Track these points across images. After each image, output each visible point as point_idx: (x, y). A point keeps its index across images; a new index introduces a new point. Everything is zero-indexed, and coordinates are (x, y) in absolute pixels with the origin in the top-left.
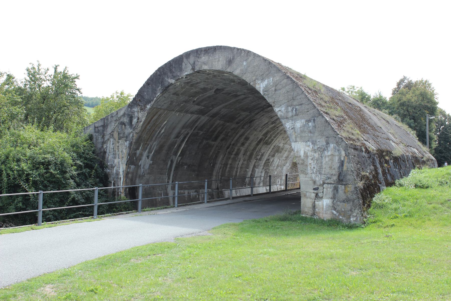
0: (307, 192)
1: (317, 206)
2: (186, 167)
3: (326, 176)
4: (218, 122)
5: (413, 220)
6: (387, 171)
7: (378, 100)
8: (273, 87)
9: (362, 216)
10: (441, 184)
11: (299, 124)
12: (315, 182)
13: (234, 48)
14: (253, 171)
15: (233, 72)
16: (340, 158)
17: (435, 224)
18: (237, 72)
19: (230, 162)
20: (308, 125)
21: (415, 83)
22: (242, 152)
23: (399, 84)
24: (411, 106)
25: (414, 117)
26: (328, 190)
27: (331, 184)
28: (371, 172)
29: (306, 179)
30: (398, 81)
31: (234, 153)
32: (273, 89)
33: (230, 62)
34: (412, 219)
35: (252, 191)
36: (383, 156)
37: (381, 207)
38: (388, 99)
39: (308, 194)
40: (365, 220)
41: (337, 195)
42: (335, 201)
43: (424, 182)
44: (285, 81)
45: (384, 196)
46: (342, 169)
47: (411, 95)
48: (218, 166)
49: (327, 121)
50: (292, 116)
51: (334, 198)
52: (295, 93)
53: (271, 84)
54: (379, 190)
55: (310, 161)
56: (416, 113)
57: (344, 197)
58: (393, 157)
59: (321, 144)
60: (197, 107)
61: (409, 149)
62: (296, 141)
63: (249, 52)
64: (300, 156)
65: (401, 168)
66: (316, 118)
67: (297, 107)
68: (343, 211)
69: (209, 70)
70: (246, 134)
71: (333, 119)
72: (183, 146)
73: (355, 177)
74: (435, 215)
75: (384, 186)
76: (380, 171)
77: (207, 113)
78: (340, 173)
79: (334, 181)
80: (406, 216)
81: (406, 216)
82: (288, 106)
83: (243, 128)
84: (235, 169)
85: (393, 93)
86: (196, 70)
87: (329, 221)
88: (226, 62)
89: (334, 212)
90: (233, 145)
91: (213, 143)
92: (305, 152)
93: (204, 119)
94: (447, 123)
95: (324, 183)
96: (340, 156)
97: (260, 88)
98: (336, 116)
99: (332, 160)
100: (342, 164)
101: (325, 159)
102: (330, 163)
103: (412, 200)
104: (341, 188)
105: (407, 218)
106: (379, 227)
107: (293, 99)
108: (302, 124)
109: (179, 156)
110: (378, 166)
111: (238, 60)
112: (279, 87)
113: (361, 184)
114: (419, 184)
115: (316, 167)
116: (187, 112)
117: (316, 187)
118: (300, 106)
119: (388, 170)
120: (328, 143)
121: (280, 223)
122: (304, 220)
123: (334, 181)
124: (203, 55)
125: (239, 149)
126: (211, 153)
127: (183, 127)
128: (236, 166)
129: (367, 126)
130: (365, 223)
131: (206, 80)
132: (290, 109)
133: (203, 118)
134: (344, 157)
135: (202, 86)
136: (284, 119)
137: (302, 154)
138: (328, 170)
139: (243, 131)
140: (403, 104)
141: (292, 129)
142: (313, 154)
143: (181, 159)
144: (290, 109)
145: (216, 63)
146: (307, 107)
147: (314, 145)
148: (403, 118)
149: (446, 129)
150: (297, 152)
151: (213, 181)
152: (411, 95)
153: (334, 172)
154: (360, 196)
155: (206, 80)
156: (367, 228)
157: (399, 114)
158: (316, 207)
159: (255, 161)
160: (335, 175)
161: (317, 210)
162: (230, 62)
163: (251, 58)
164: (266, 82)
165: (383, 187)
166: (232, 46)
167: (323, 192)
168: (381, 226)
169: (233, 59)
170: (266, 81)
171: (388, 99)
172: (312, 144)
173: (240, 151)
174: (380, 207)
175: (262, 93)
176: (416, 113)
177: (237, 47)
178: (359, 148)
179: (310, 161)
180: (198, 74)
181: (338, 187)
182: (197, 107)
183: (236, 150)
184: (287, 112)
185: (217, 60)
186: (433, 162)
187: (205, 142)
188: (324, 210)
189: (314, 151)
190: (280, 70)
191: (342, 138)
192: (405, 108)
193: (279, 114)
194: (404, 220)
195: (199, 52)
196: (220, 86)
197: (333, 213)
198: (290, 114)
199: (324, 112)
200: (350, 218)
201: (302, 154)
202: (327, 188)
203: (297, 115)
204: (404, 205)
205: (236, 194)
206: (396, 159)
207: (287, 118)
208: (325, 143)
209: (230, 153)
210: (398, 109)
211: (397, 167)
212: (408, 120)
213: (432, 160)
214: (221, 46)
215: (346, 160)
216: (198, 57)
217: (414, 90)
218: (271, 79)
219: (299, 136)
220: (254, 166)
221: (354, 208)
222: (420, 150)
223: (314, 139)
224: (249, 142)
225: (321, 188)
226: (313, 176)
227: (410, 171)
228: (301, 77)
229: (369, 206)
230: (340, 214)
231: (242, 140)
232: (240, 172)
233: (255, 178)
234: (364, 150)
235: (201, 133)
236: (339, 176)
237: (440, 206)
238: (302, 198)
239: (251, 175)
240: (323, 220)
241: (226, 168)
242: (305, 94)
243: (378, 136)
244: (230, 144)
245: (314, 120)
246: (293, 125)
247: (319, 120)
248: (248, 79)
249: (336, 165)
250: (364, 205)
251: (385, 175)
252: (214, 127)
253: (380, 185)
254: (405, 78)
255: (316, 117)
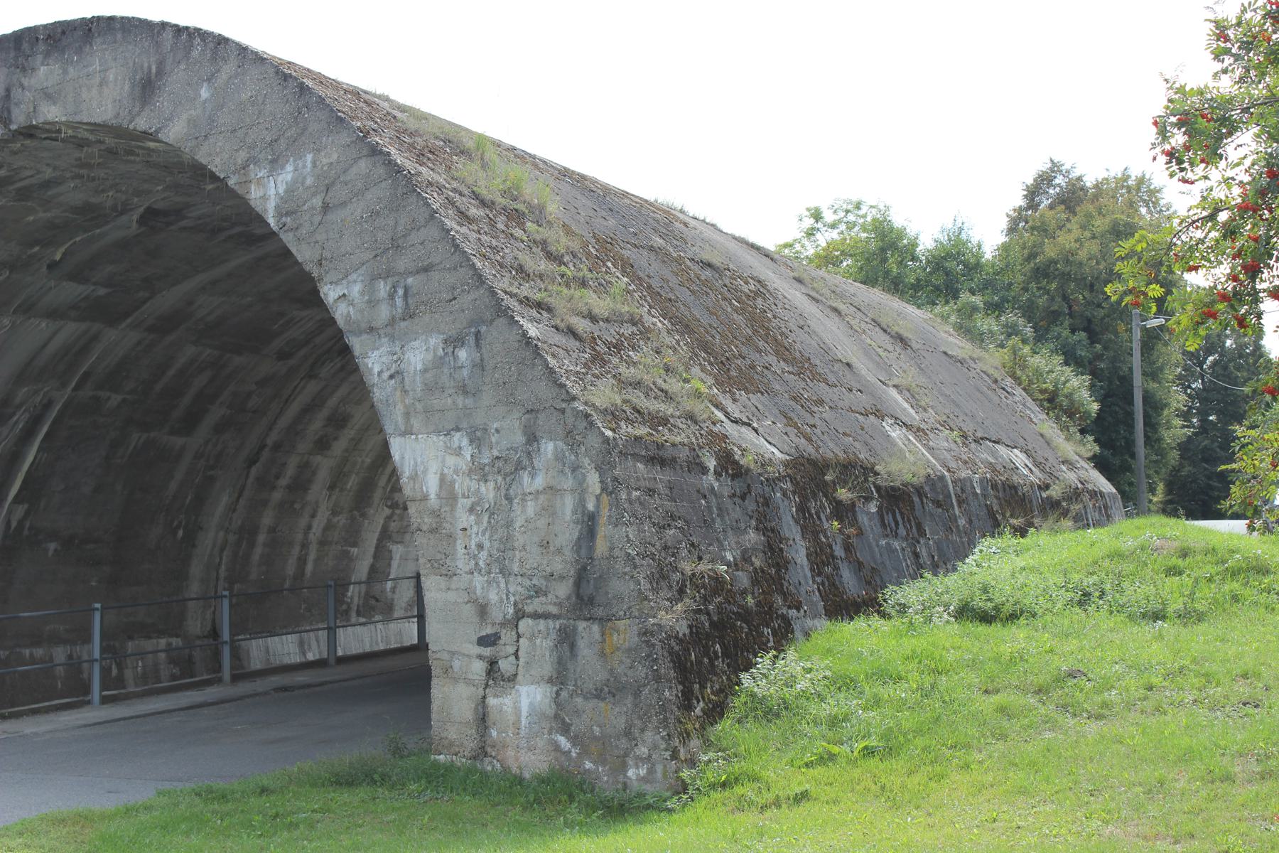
0: (453, 653)
1: (493, 716)
2: (52, 546)
3: (527, 583)
4: (190, 351)
5: (892, 772)
6: (839, 551)
7: (948, 256)
8: (314, 195)
9: (675, 756)
10: (1084, 599)
11: (417, 356)
12: (483, 611)
13: (164, 25)
14: (381, 553)
15: (157, 132)
16: (582, 502)
17: (981, 788)
18: (174, 133)
19: (267, 519)
20: (455, 358)
21: (1096, 186)
22: (323, 476)
23: (1033, 193)
24: (1075, 280)
25: (1089, 321)
26: (537, 643)
27: (546, 616)
28: (746, 558)
29: (451, 596)
30: (1030, 181)
31: (283, 482)
32: (317, 202)
33: (147, 88)
34: (899, 764)
35: (332, 642)
36: (827, 490)
37: (767, 712)
38: (988, 253)
39: (456, 664)
40: (686, 774)
41: (570, 666)
42: (564, 694)
43: (1005, 593)
44: (363, 165)
45: (813, 662)
46: (591, 549)
47: (1076, 232)
48: (209, 540)
49: (526, 340)
50: (392, 322)
51: (559, 679)
52: (402, 222)
53: (309, 181)
54: (784, 636)
55: (464, 519)
56: (1099, 306)
57: (601, 676)
58: (878, 488)
59: (504, 444)
60: (72, 291)
61: (984, 454)
62: (407, 432)
63: (222, 41)
64: (425, 498)
65: (922, 533)
66: (483, 329)
67: (410, 280)
68: (595, 738)
69: (68, 124)
70: (332, 402)
71: (572, 332)
72: (30, 459)
73: (645, 585)
74: (1000, 745)
75: (815, 616)
76: (799, 552)
77: (127, 315)
78: (584, 568)
79: (560, 605)
80: (869, 752)
81: (869, 752)
82: (374, 278)
83: (311, 376)
84: (296, 550)
85: (1012, 230)
86: (14, 127)
87: (543, 781)
88: (133, 86)
89: (563, 741)
90: (277, 447)
91: (179, 441)
92: (442, 479)
93: (118, 340)
94: (1229, 343)
95: (520, 615)
96: (581, 491)
97: (265, 198)
98: (593, 318)
99: (549, 511)
100: (589, 525)
101: (524, 507)
102: (542, 523)
103: (914, 679)
104: (587, 632)
105: (873, 763)
106: (742, 805)
107: (396, 246)
108: (430, 357)
109: (17, 500)
110: (791, 529)
111: (177, 76)
112: (340, 193)
113: (674, 618)
114: (979, 603)
115: (487, 544)
116: (28, 309)
117: (489, 630)
118: (422, 277)
119: (848, 548)
120: (532, 438)
121: (344, 796)
122: (440, 780)
123: (560, 605)
124: (40, 57)
125: (304, 466)
126: (173, 486)
127: (21, 377)
128: (300, 536)
129: (772, 359)
130: (685, 790)
131: (83, 172)
132: (383, 288)
133: (111, 335)
134: (598, 498)
135: (72, 194)
136: (359, 333)
137: (432, 485)
138: (534, 558)
139: (312, 387)
140: (1042, 273)
141: (391, 377)
142: (474, 485)
143: (27, 513)
144: (383, 288)
145: (94, 91)
146: (450, 279)
147: (479, 447)
148: (1042, 326)
149: (1225, 368)
150: (414, 477)
151: (191, 604)
152: (1076, 232)
153: (558, 566)
154: (666, 669)
155: (83, 172)
156: (689, 814)
157: (1028, 312)
158: (490, 723)
159: (387, 511)
160: (562, 578)
161: (494, 733)
162: (147, 88)
163: (228, 69)
164: (287, 174)
165: (809, 622)
166: (154, 14)
167: (516, 655)
168: (751, 803)
169: (160, 73)
170: (289, 168)
171: (988, 253)
172: (471, 441)
173: (314, 473)
174: (766, 714)
175: (272, 221)
176: (1099, 306)
177: (174, 22)
178: (683, 454)
179: (464, 519)
180: (28, 142)
181: (575, 629)
182: (72, 291)
183: (290, 471)
184: (373, 303)
185: (98, 80)
186: (1100, 504)
187: (136, 438)
188: (523, 733)
189: (480, 472)
190: (341, 119)
191: (587, 416)
192: (1054, 286)
193: (341, 313)
194: (856, 773)
195: (25, 46)
196: (159, 196)
197: (557, 748)
198: (384, 312)
199: (526, 302)
200: (624, 767)
201: (432, 485)
202: (532, 638)
203: (409, 315)
204: (877, 702)
205: (304, 654)
206: (899, 501)
207: (371, 330)
208: (520, 439)
209: (265, 483)
210: (1026, 289)
211: (902, 531)
212: (1066, 333)
213: (1094, 494)
214: (111, 19)
215: (605, 512)
216: (24, 70)
217: (1089, 216)
218: (309, 157)
219: (419, 406)
220: (385, 535)
221: (638, 723)
222: (1042, 453)
223: (479, 419)
224: (349, 433)
225: (507, 636)
226: (479, 581)
227: (972, 544)
228: (450, 145)
229: (716, 712)
230: (585, 753)
231: (316, 425)
232: (318, 560)
233: (389, 584)
234: (711, 464)
235: (116, 399)
236: (578, 584)
237: (1032, 700)
238: (434, 682)
239: (373, 570)
240: (520, 780)
241: (252, 544)
242: (443, 224)
243: (820, 402)
244: (263, 447)
245: (478, 335)
246: (394, 363)
247: (497, 335)
248: (217, 161)
249: (567, 534)
250: (688, 707)
251: (828, 570)
252: (171, 372)
253: (793, 613)
254: (1055, 167)
255: (483, 322)
